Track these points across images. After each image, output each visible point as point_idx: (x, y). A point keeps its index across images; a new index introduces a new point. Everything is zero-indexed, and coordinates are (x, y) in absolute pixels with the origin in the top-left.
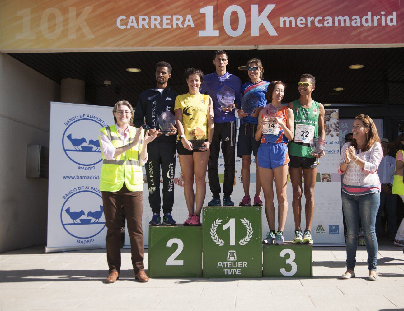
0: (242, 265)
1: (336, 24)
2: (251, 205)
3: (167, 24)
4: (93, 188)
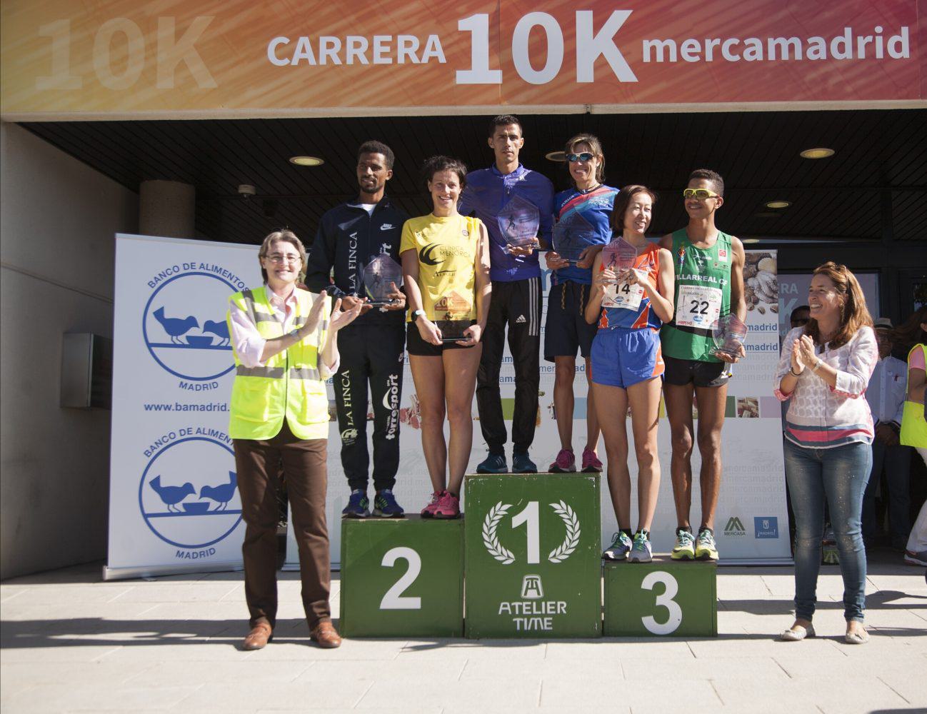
0: (556, 610)
1: (772, 56)
2: (575, 471)
3: (383, 55)
4: (213, 431)
